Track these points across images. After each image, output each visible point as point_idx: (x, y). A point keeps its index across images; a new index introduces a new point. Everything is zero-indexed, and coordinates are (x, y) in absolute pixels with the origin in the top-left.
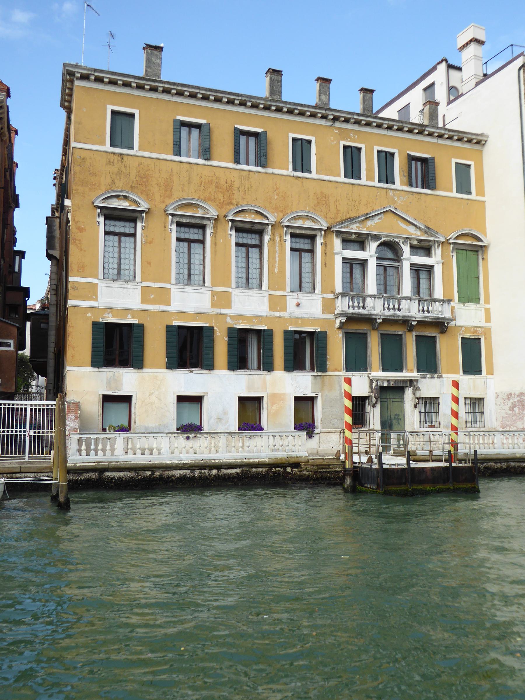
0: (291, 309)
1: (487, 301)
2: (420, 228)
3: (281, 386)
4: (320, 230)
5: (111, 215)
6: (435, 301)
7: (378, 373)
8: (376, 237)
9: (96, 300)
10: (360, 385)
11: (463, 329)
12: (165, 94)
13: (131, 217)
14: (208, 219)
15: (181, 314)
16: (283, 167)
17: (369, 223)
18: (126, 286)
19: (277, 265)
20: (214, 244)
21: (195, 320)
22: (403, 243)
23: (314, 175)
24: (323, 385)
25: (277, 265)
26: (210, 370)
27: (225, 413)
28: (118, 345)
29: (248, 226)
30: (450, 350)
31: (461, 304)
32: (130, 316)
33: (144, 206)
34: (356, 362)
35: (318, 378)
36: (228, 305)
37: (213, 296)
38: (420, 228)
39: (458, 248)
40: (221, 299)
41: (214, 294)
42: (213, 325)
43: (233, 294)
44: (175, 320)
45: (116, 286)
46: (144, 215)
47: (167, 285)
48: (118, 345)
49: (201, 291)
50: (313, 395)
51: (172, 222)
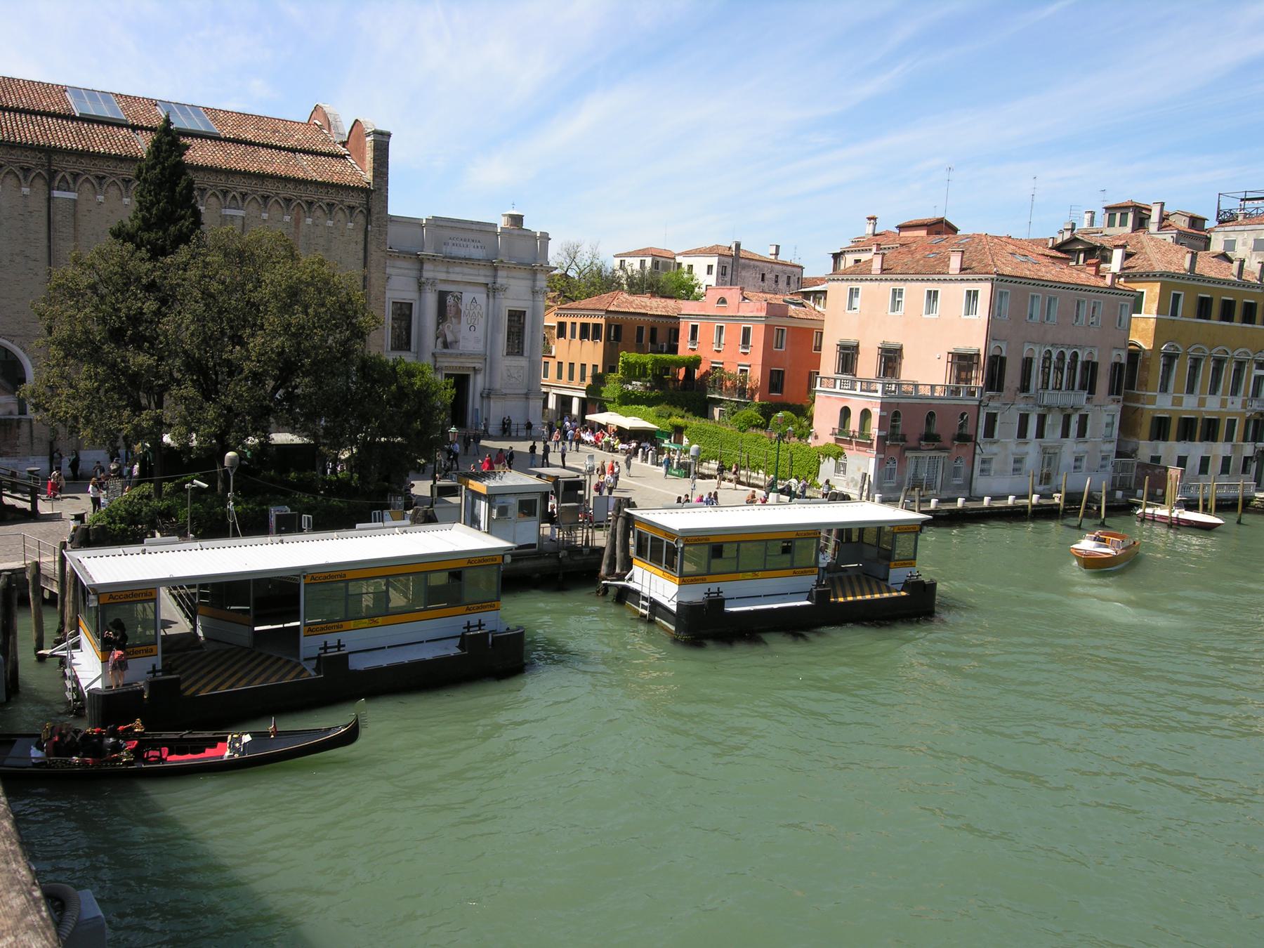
0: (1229, 405)
15: (1185, 412)
28: (1160, 429)
48: (1160, 429)
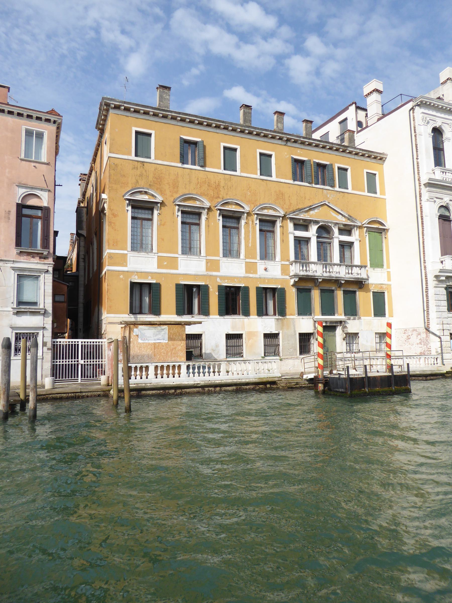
1: (388, 267)
2: (345, 216)
3: (254, 326)
4: (279, 217)
5: (136, 205)
6: (335, 265)
7: (319, 317)
8: (316, 222)
9: (126, 266)
10: (306, 325)
11: (374, 286)
12: (173, 120)
13: (149, 207)
14: (203, 208)
15: (185, 275)
16: (215, 166)
17: (312, 212)
18: (147, 256)
19: (250, 241)
20: (208, 226)
21: (195, 280)
22: (334, 227)
23: (238, 173)
24: (283, 325)
25: (250, 241)
26: (206, 315)
27: (217, 346)
29: (230, 214)
30: (364, 300)
31: (372, 269)
32: (150, 278)
33: (159, 199)
34: (305, 309)
35: (279, 320)
36: (218, 270)
37: (207, 263)
38: (345, 216)
39: (369, 230)
40: (213, 265)
41: (208, 261)
42: (207, 283)
43: (179, 259)
44: (181, 280)
45: (140, 256)
46: (159, 205)
47: (176, 255)
48: (144, 296)
49: (199, 259)
50: (277, 332)
51: (178, 210)
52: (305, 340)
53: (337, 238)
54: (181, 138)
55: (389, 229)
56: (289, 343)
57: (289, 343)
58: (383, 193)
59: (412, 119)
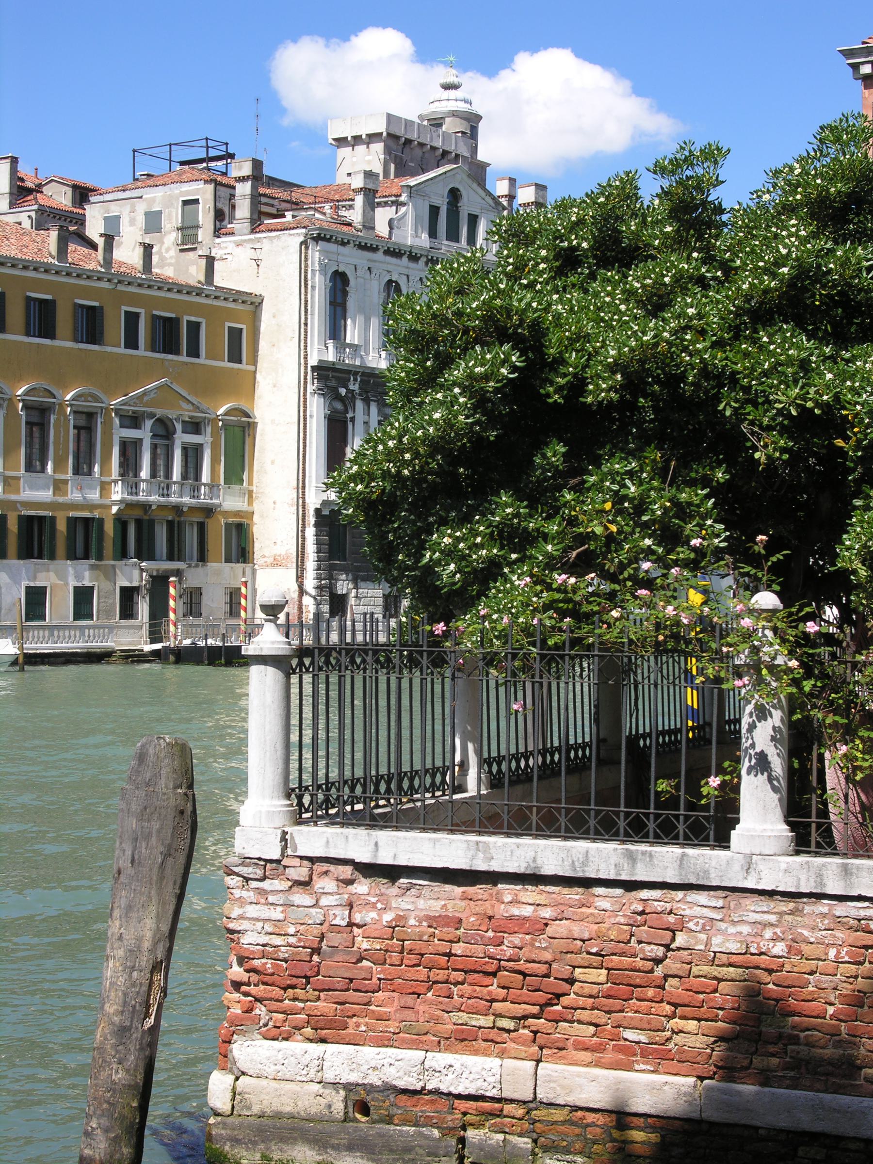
8: (152, 415)
50: (90, 584)
52: (128, 595)
53: (181, 438)
54: (29, 299)
55: (389, 117)
56: (107, 600)
57: (107, 600)
58: (254, 361)
59: (304, 260)
